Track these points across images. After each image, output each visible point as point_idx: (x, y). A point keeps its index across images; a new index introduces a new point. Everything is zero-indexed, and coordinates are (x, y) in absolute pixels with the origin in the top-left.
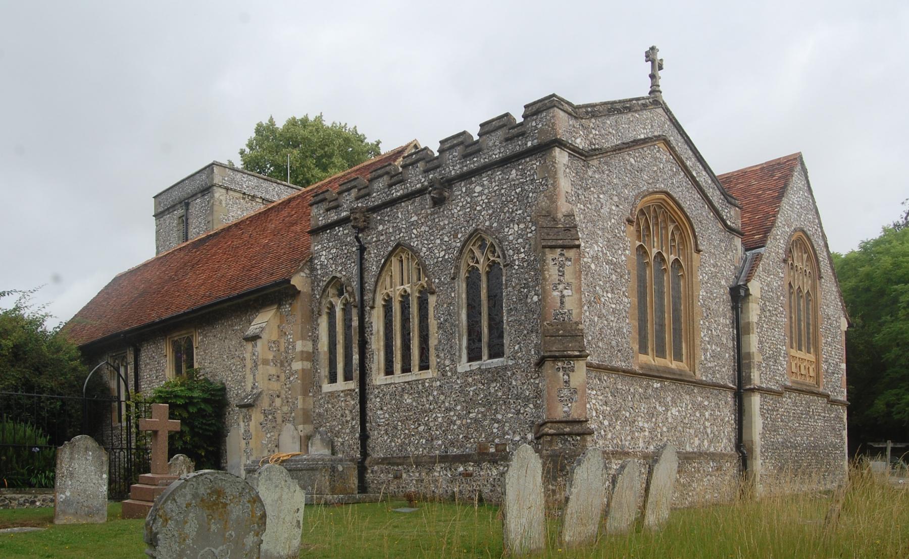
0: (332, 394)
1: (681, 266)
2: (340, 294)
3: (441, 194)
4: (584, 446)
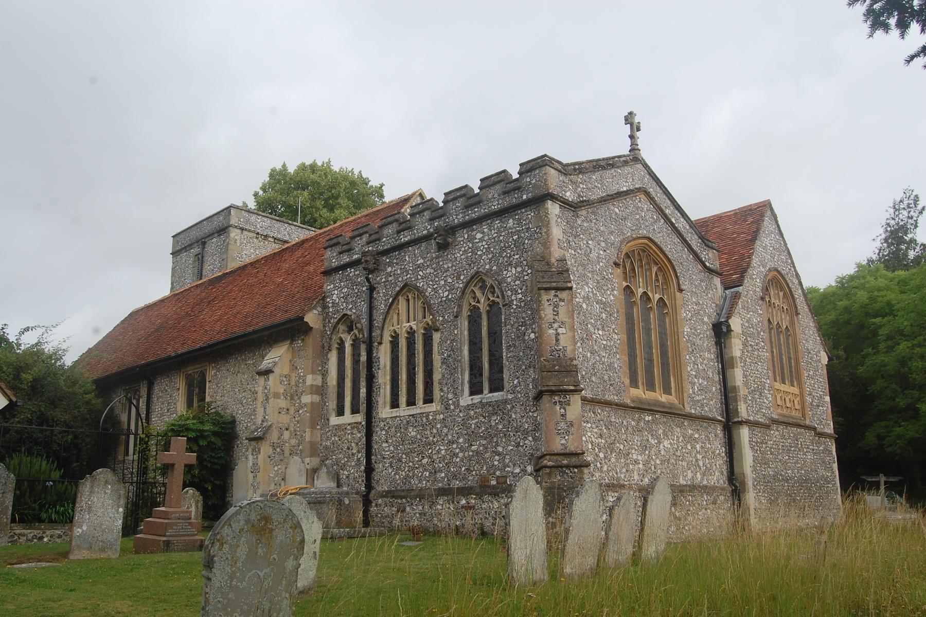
0: (339, 427)
1: (665, 304)
2: (350, 329)
3: (445, 240)
4: (582, 478)
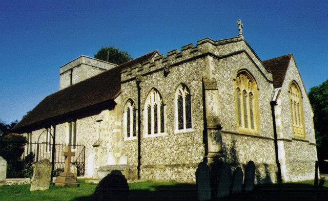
0: (128, 141)
